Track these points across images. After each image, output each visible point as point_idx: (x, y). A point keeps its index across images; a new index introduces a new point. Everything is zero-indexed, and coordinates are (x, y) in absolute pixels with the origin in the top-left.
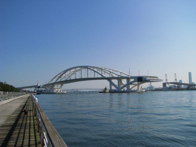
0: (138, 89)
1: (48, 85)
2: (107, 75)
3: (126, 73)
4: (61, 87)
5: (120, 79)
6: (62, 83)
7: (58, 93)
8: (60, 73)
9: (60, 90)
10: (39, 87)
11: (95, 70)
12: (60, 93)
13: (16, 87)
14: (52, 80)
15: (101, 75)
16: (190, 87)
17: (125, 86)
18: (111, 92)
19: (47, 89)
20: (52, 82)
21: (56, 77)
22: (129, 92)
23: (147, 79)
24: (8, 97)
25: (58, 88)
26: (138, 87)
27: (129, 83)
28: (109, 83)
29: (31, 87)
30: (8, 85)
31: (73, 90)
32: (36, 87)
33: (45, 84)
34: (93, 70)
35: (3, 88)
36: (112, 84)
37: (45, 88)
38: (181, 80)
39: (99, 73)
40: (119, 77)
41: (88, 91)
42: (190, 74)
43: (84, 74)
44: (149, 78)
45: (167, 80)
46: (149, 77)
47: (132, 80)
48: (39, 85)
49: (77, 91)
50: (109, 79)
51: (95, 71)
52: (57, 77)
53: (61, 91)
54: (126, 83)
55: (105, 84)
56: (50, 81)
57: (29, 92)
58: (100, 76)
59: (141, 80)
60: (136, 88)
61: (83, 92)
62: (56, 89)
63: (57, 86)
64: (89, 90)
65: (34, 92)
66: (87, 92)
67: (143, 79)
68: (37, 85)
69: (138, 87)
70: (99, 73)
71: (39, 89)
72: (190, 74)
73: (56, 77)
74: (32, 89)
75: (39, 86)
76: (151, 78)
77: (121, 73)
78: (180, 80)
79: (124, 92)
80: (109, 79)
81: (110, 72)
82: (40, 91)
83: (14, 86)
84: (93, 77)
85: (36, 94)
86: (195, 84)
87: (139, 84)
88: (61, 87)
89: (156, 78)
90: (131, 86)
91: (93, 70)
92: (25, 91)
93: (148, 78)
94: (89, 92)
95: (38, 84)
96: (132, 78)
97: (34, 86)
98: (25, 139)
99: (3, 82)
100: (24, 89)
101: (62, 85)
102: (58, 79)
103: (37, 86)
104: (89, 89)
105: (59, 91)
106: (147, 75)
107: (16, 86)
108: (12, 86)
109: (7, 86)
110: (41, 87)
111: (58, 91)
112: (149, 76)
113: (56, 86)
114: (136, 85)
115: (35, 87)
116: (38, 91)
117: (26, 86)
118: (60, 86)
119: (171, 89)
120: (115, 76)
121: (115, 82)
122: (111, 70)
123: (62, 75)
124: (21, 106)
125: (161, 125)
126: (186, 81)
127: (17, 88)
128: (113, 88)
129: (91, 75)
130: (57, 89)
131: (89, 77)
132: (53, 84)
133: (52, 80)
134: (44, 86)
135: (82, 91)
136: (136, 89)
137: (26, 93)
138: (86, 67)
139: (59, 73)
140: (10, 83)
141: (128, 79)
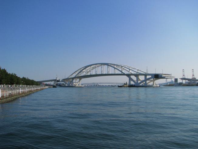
0: (154, 85)
1: (68, 79)
2: (126, 73)
3: (144, 71)
4: (79, 81)
5: (137, 75)
6: (81, 78)
7: (80, 87)
8: (80, 69)
9: (78, 83)
10: (58, 81)
11: (115, 67)
12: (78, 87)
13: (36, 81)
14: (72, 75)
16: (192, 83)
17: (142, 81)
18: (131, 86)
19: (66, 83)
20: (71, 77)
21: (76, 72)
22: (146, 86)
23: (163, 76)
24: (14, 89)
25: (76, 82)
26: (154, 83)
27: (146, 80)
28: (128, 79)
29: (51, 81)
30: (30, 80)
31: (93, 83)
32: (56, 81)
33: (64, 78)
34: (114, 67)
36: (131, 79)
37: (65, 82)
39: (119, 70)
40: (138, 73)
41: (107, 85)
43: (105, 70)
44: (164, 76)
45: (194, 75)
46: (164, 74)
47: (148, 77)
48: (58, 79)
49: (97, 85)
50: (128, 75)
51: (115, 68)
52: (77, 73)
53: (79, 85)
54: (144, 79)
55: (125, 80)
56: (70, 75)
58: (120, 73)
59: (157, 76)
60: (151, 84)
61: (103, 86)
62: (75, 83)
63: (79, 80)
66: (106, 86)
67: (159, 76)
68: (56, 79)
69: (154, 83)
70: (119, 70)
71: (58, 83)
73: (76, 72)
74: (52, 83)
75: (58, 80)
76: (166, 76)
77: (138, 70)
79: (142, 86)
80: (128, 75)
81: (130, 69)
82: (58, 84)
84: (113, 73)
86: (197, 79)
87: (154, 80)
88: (79, 81)
89: (170, 76)
90: (148, 81)
91: (114, 67)
93: (163, 76)
94: (108, 86)
95: (57, 78)
99: (26, 78)
100: (45, 83)
101: (80, 79)
104: (112, 83)
105: (77, 84)
106: (162, 73)
107: (36, 79)
108: (32, 80)
109: (29, 80)
110: (61, 80)
111: (76, 85)
112: (164, 73)
113: (74, 81)
114: (152, 81)
115: (54, 81)
116: (57, 85)
117: (44, 80)
118: (78, 80)
119: (181, 85)
120: (133, 73)
121: (134, 78)
122: (130, 67)
123: (82, 71)
125: (118, 113)
127: (38, 82)
128: (132, 83)
129: (111, 70)
130: (76, 83)
131: (115, 73)
132: (73, 79)
133: (72, 75)
135: (101, 85)
136: (151, 85)
138: (107, 64)
140: (31, 78)
141: (146, 75)
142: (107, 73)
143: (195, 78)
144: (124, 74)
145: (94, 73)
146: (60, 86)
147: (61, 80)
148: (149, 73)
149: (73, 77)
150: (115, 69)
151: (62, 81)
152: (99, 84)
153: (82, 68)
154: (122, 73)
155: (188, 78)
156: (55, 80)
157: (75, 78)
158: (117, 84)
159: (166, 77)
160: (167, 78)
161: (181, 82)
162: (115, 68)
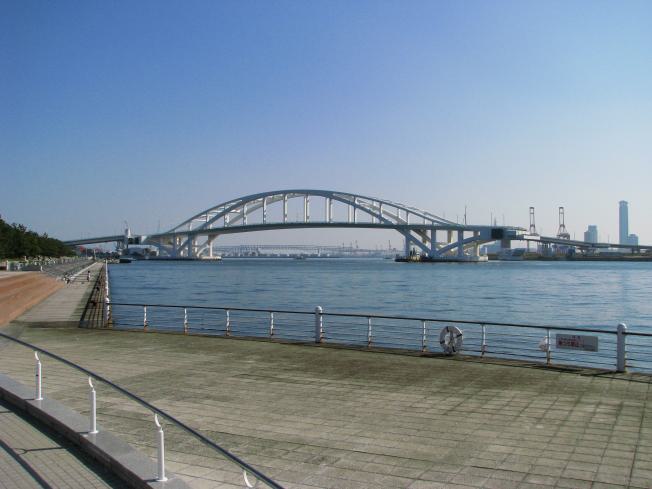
7: (209, 260)
8: (224, 204)
14: (189, 221)
15: (379, 217)
16: (632, 254)
17: (454, 246)
20: (185, 228)
21: (206, 212)
27: (461, 242)
31: (242, 248)
35: (43, 249)
36: (409, 239)
38: (595, 227)
41: (288, 252)
42: (623, 208)
43: (317, 210)
45: (564, 226)
47: (468, 235)
48: (129, 236)
50: (403, 228)
52: (211, 216)
55: (395, 241)
57: (102, 255)
58: (376, 220)
64: (293, 252)
65: (116, 256)
68: (123, 233)
71: (130, 246)
72: (623, 208)
73: (206, 212)
74: (111, 247)
78: (590, 227)
80: (403, 228)
82: (131, 252)
83: (30, 227)
85: (118, 261)
88: (208, 243)
92: (90, 253)
93: (519, 233)
95: (127, 231)
96: (469, 229)
97: (115, 237)
98: (615, 406)
100: (87, 246)
102: (213, 220)
103: (123, 236)
107: (63, 236)
110: (143, 238)
115: (118, 241)
116: (126, 252)
117: (92, 237)
119: (521, 258)
122: (426, 213)
124: (86, 294)
126: (609, 236)
129: (341, 212)
132: (192, 235)
134: (155, 239)
137: (93, 259)
139: (221, 203)
141: (461, 229)
142: (280, 221)
143: (568, 236)
144: (389, 226)
145: (260, 221)
146: (138, 256)
147: (143, 238)
148: (471, 222)
149: (191, 229)
150: (357, 210)
151: (148, 241)
152: (262, 252)
153: (233, 201)
154: (383, 223)
155: (117, 234)
156: (121, 239)
157: (202, 231)
158: (318, 248)
159: (525, 237)
160: (528, 240)
161: (526, 247)
162: (356, 206)
